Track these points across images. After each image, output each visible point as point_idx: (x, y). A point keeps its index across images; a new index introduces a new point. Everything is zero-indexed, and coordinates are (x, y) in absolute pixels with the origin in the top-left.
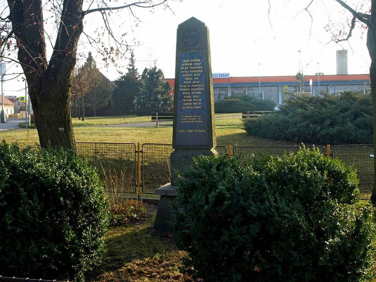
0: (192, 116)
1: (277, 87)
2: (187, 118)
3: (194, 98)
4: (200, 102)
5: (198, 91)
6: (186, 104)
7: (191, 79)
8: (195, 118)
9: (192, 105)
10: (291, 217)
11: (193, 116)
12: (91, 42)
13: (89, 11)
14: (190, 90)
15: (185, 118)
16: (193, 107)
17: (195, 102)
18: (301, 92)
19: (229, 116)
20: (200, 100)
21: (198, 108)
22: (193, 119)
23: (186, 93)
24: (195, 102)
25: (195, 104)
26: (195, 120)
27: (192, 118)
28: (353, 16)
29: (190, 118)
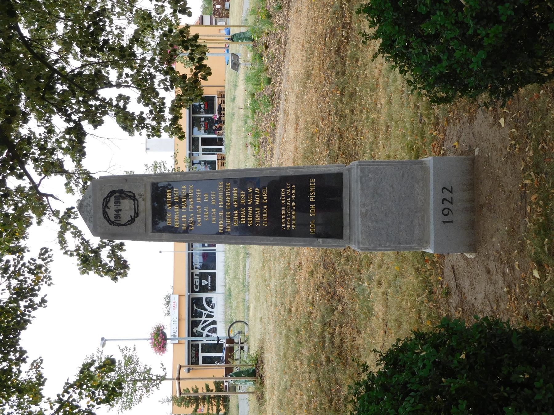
0: (283, 206)
1: (209, 24)
2: (286, 217)
3: (246, 202)
4: (254, 190)
5: (232, 194)
6: (258, 219)
7: (213, 203)
8: (286, 200)
9: (261, 205)
10: (547, 103)
11: (283, 204)
12: (181, 377)
13: (149, 339)
14: (229, 210)
15: (286, 221)
16: (265, 204)
17: (254, 199)
18: (203, 150)
19: (285, 112)
20: (250, 190)
21: (265, 195)
22: (288, 204)
23: (236, 218)
24: (254, 199)
25: (258, 201)
26: (291, 201)
27: (285, 206)
28: (97, 176)
29: (286, 212)
